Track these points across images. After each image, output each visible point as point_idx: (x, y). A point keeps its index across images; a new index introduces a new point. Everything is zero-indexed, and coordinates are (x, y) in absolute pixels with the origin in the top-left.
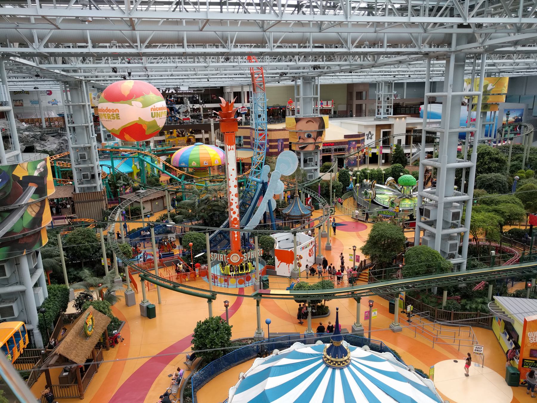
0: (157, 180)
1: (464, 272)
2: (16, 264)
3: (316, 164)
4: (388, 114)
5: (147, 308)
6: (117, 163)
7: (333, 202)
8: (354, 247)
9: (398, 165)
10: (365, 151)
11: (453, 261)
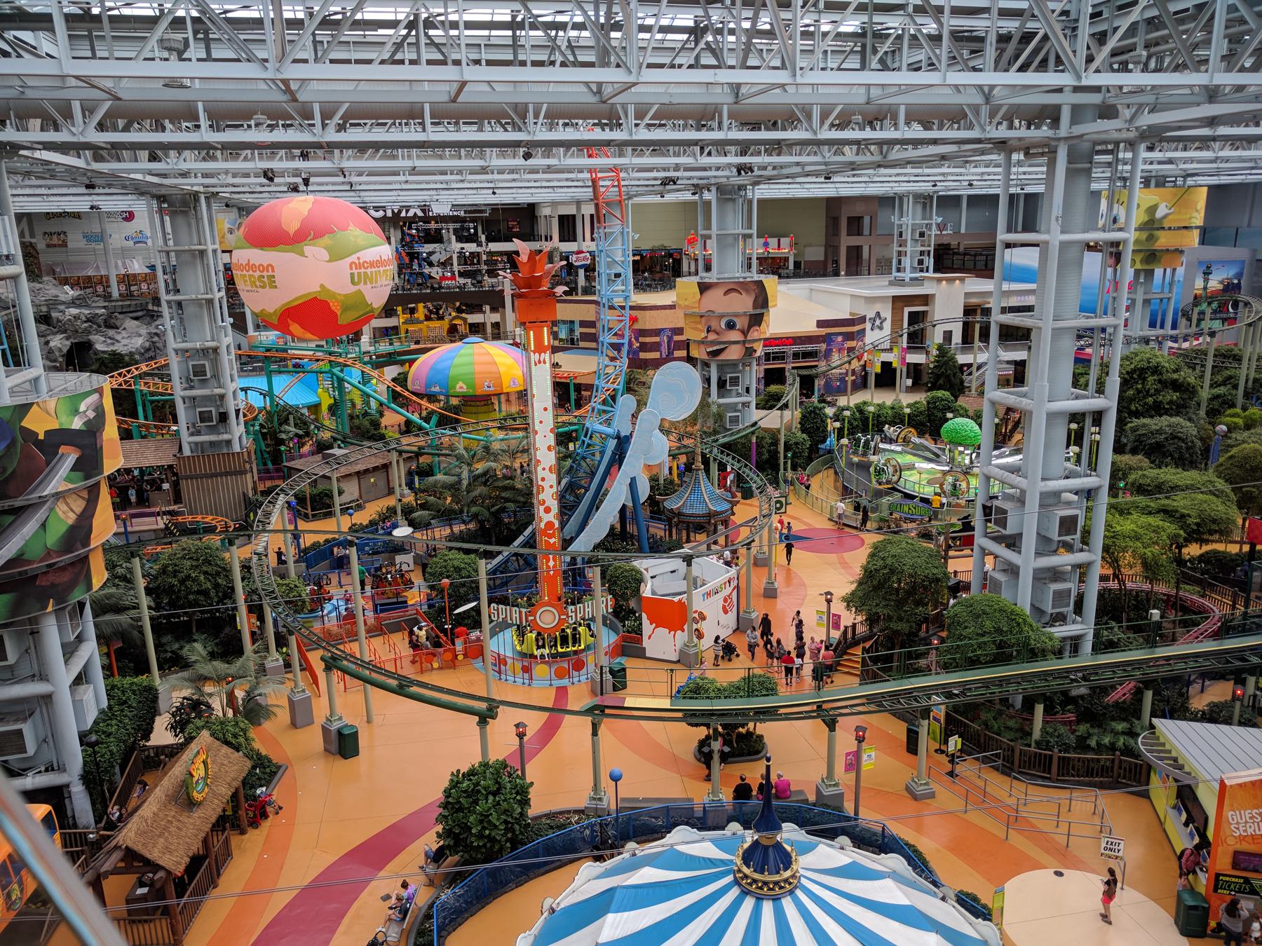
0: (376, 424)
1: (1087, 658)
2: (32, 633)
3: (748, 390)
4: (922, 271)
5: (339, 733)
6: (281, 383)
7: (786, 481)
8: (828, 593)
9: (940, 393)
10: (865, 357)
11: (1059, 631)
